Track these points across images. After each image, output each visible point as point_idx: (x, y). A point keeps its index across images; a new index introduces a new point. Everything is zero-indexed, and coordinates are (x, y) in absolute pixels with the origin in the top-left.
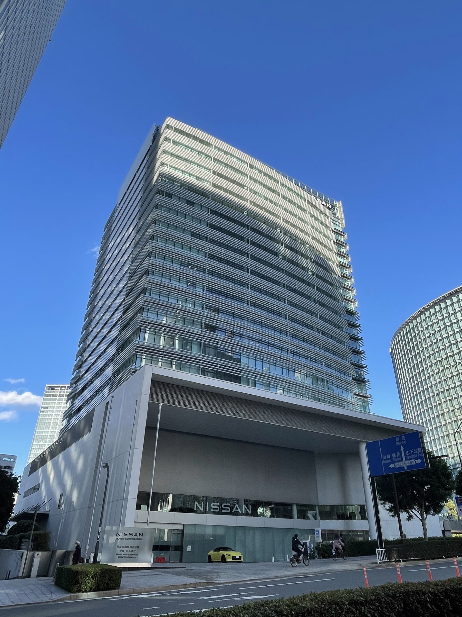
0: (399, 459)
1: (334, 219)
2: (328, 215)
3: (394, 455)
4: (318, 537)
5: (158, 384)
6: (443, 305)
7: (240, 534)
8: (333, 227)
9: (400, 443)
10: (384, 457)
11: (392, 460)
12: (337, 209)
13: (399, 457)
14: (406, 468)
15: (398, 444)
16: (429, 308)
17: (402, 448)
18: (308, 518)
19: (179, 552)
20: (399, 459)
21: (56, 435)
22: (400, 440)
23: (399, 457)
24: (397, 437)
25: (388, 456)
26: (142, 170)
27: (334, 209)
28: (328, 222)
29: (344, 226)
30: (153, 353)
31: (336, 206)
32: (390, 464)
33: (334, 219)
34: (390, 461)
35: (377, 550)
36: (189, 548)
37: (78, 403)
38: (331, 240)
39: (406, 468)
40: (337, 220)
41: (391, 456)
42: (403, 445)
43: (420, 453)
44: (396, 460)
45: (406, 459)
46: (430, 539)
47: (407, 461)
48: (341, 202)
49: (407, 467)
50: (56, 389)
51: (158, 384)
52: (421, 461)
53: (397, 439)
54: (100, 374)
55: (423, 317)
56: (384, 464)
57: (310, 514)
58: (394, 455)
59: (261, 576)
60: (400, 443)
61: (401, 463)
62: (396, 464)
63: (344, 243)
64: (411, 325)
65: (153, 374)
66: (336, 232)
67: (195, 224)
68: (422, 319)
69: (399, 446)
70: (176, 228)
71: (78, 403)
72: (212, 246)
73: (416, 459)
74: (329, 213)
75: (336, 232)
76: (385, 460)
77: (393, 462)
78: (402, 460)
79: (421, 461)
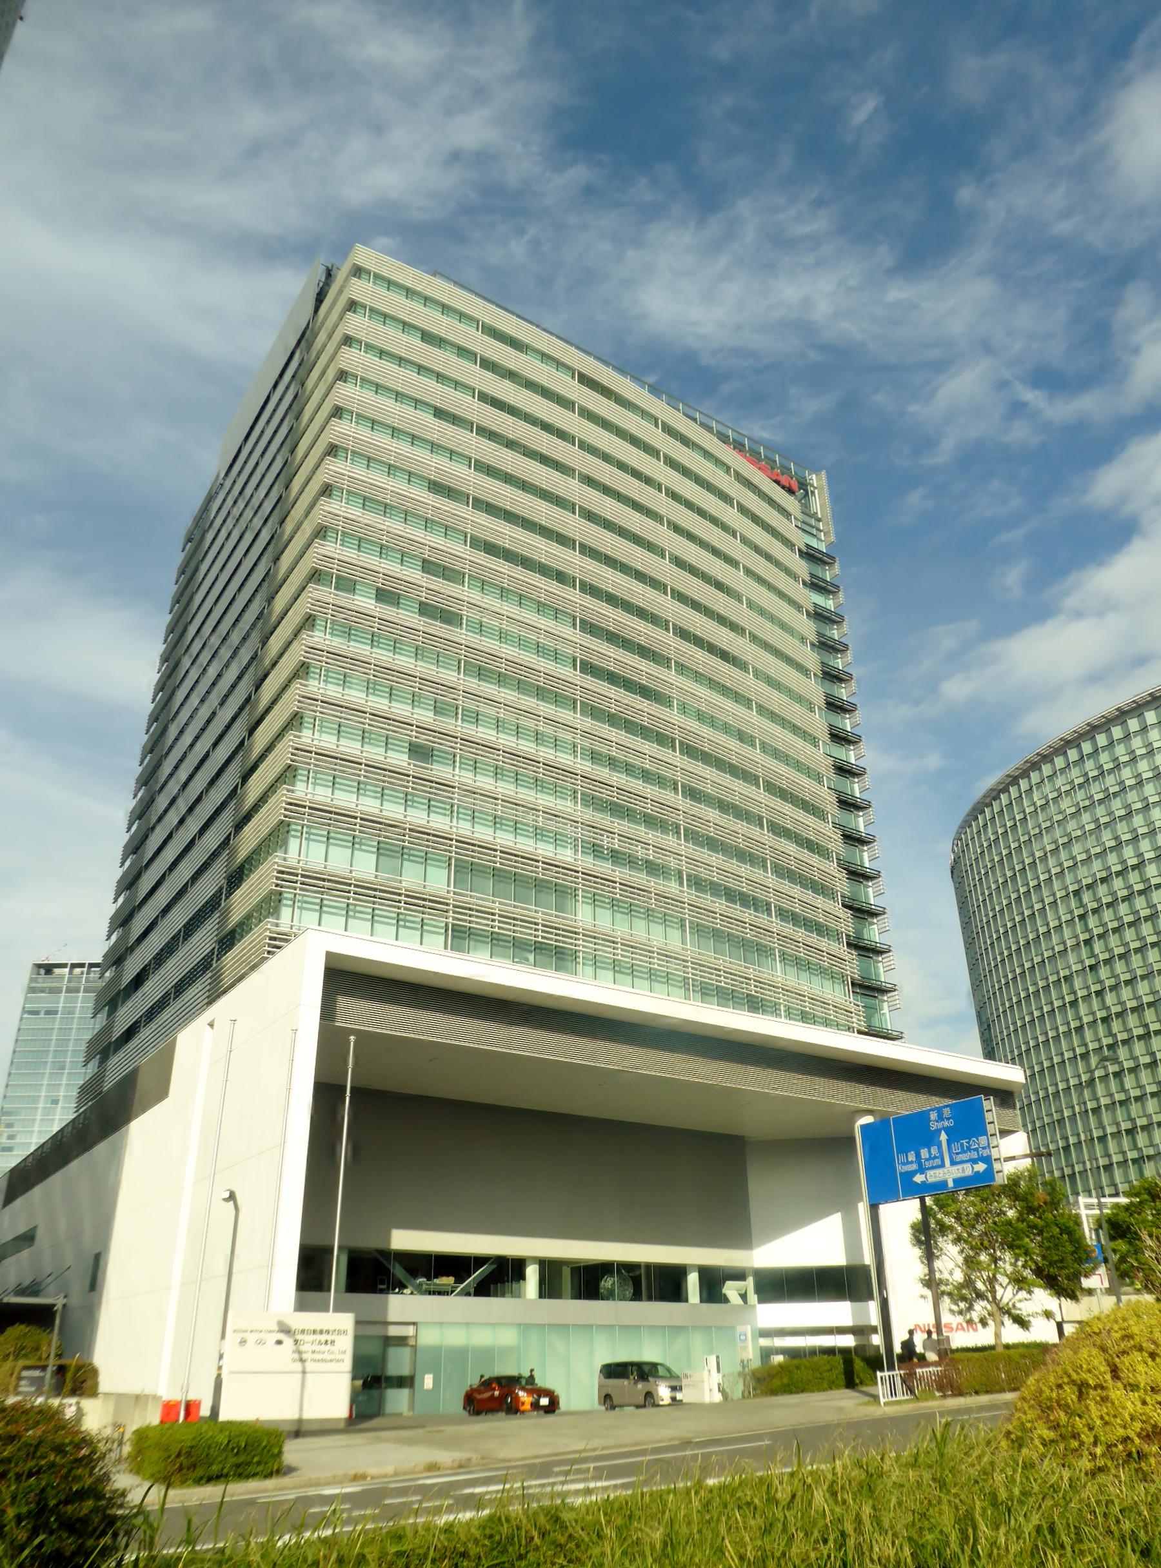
0: (938, 1162)
1: (807, 519)
2: (789, 508)
3: (924, 1153)
4: (745, 1348)
5: (344, 979)
6: (1087, 748)
7: (993, 982)
8: (801, 540)
9: (940, 1125)
10: (902, 1157)
11: (920, 1164)
12: (813, 493)
13: (935, 1157)
14: (951, 1184)
15: (934, 1126)
16: (1052, 754)
17: (943, 1137)
18: (725, 1300)
19: (231, 1203)
20: (938, 1162)
21: (62, 1093)
22: (941, 1118)
23: (935, 1157)
24: (932, 1110)
25: (912, 1157)
26: (287, 388)
27: (806, 491)
28: (789, 529)
29: (832, 538)
30: (325, 887)
31: (812, 485)
32: (914, 1173)
33: (807, 519)
34: (914, 1167)
35: (879, 1374)
36: (428, 1381)
37: (128, 1013)
38: (795, 578)
39: (951, 1184)
40: (813, 522)
41: (918, 1155)
42: (948, 1131)
43: (984, 1148)
44: (927, 1165)
45: (953, 1163)
46: (1007, 1347)
47: (955, 1168)
48: (823, 473)
49: (955, 1181)
50: (57, 971)
51: (344, 979)
52: (985, 1166)
53: (933, 1116)
54: (185, 939)
55: (1035, 777)
56: (901, 1174)
57: (731, 1289)
58: (924, 1153)
59: (605, 1443)
60: (940, 1125)
61: (941, 1171)
62: (930, 1173)
63: (833, 585)
64: (1013, 790)
65: (330, 956)
66: (810, 555)
67: (436, 540)
68: (1033, 783)
69: (938, 1131)
70: (383, 550)
71: (128, 1013)
72: (483, 519)
73: (974, 1161)
74: (790, 503)
75: (810, 555)
76: (904, 1164)
77: (922, 1170)
78: (943, 1165)
79: (985, 1166)
